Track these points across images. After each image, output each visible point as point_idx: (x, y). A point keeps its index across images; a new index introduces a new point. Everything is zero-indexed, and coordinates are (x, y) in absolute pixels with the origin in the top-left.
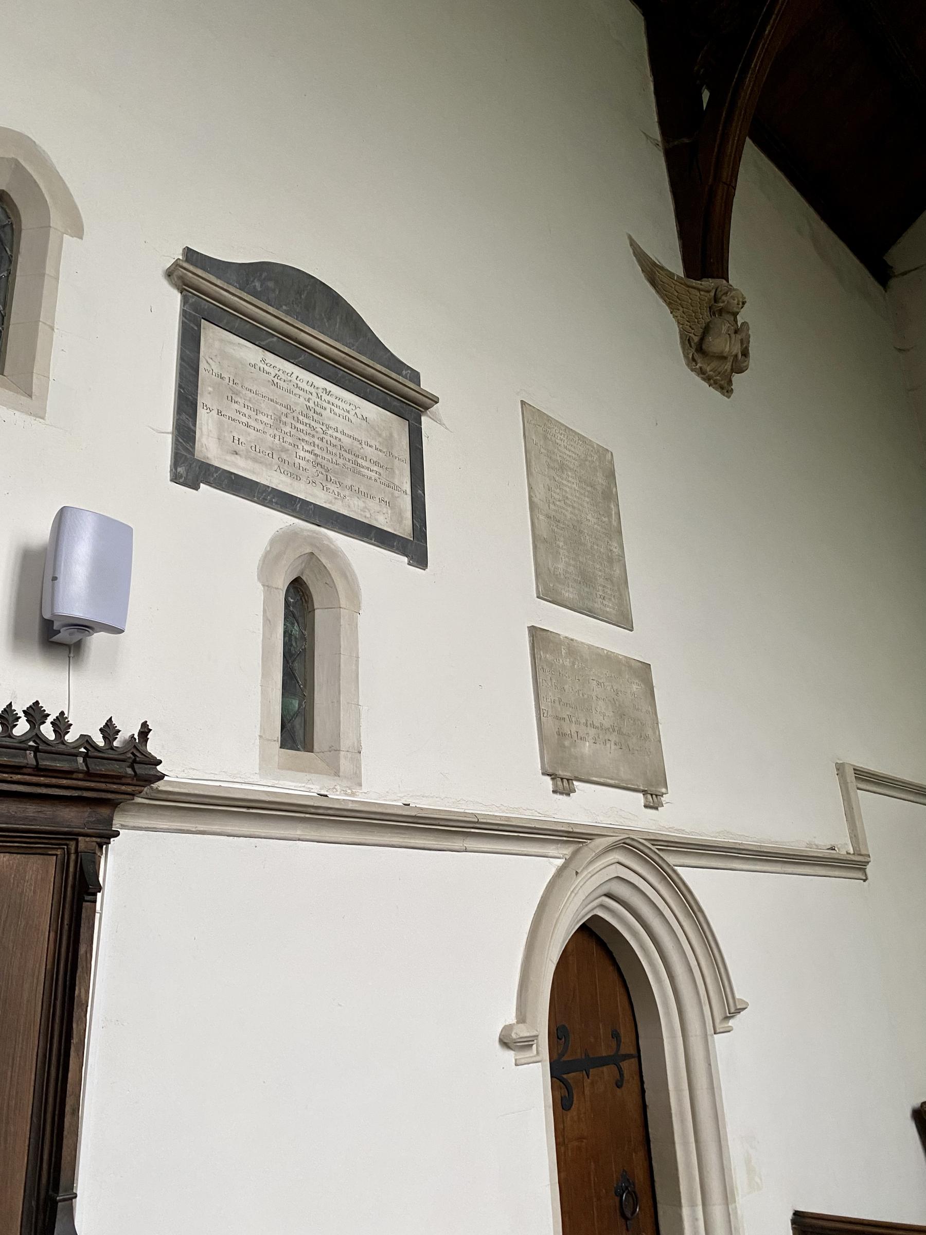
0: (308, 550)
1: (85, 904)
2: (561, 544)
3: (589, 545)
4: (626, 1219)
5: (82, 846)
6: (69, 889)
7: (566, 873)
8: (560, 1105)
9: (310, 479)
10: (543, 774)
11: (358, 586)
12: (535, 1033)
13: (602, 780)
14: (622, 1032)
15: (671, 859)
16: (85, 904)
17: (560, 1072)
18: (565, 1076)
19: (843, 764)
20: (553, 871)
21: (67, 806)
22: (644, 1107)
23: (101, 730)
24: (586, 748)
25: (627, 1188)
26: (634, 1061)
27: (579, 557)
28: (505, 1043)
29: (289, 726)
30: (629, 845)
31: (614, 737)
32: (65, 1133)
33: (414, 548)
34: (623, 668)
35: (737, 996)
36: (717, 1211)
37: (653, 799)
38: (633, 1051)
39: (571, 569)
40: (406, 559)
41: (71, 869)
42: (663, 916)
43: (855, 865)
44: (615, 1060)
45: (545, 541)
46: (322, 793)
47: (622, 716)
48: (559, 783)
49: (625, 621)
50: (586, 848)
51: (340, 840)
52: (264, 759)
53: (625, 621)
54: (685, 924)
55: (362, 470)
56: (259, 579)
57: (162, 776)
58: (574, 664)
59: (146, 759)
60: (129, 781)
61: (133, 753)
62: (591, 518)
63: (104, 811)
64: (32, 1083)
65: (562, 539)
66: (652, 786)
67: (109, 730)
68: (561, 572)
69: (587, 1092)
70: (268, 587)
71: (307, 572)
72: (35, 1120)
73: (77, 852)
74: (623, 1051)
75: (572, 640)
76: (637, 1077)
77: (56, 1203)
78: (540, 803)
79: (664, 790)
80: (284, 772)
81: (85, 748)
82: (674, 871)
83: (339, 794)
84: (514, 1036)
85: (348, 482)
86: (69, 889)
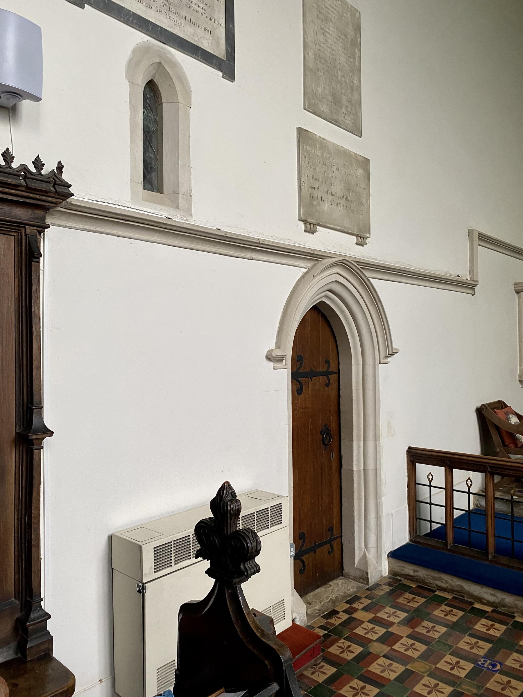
0: (157, 61)
1: (33, 263)
2: (322, 74)
3: (340, 77)
4: (325, 445)
5: (28, 231)
6: (23, 255)
7: (307, 276)
8: (296, 393)
9: (158, 8)
10: (299, 220)
11: (190, 89)
12: (285, 354)
13: (333, 226)
14: (331, 362)
15: (368, 274)
16: (33, 263)
17: (296, 376)
18: (299, 379)
19: (473, 230)
20: (301, 274)
21: (17, 207)
22: (339, 396)
23: (33, 162)
24: (326, 207)
25: (327, 431)
26: (337, 375)
27: (332, 89)
28: (269, 358)
29: (148, 177)
30: (344, 264)
31: (343, 202)
32: (34, 378)
33: (226, 66)
34: (353, 160)
35: (394, 347)
36: (371, 444)
37: (362, 240)
38: (336, 370)
39: (327, 92)
40: (221, 74)
41: (24, 244)
42: (359, 303)
43: (469, 286)
44: (327, 374)
45: (311, 70)
46: (169, 217)
47: (349, 189)
48: (308, 226)
49: (357, 131)
50: (320, 264)
51: (180, 245)
52: (133, 193)
53: (357, 131)
54: (370, 308)
55: (193, 5)
56: (126, 76)
57: (72, 195)
58: (323, 154)
59: (62, 183)
60: (53, 195)
61: (53, 179)
62: (342, 59)
63: (40, 213)
64: (14, 357)
65: (322, 70)
66: (361, 232)
67: (38, 163)
68: (321, 94)
69: (310, 387)
70: (132, 83)
71: (157, 77)
72: (17, 371)
73: (26, 235)
74: (330, 370)
75: (324, 139)
76: (337, 383)
77: (32, 410)
78: (296, 236)
79: (368, 235)
80: (146, 203)
81: (24, 172)
82: (368, 280)
83: (178, 219)
84: (273, 355)
85: (184, 14)
86: (23, 255)
